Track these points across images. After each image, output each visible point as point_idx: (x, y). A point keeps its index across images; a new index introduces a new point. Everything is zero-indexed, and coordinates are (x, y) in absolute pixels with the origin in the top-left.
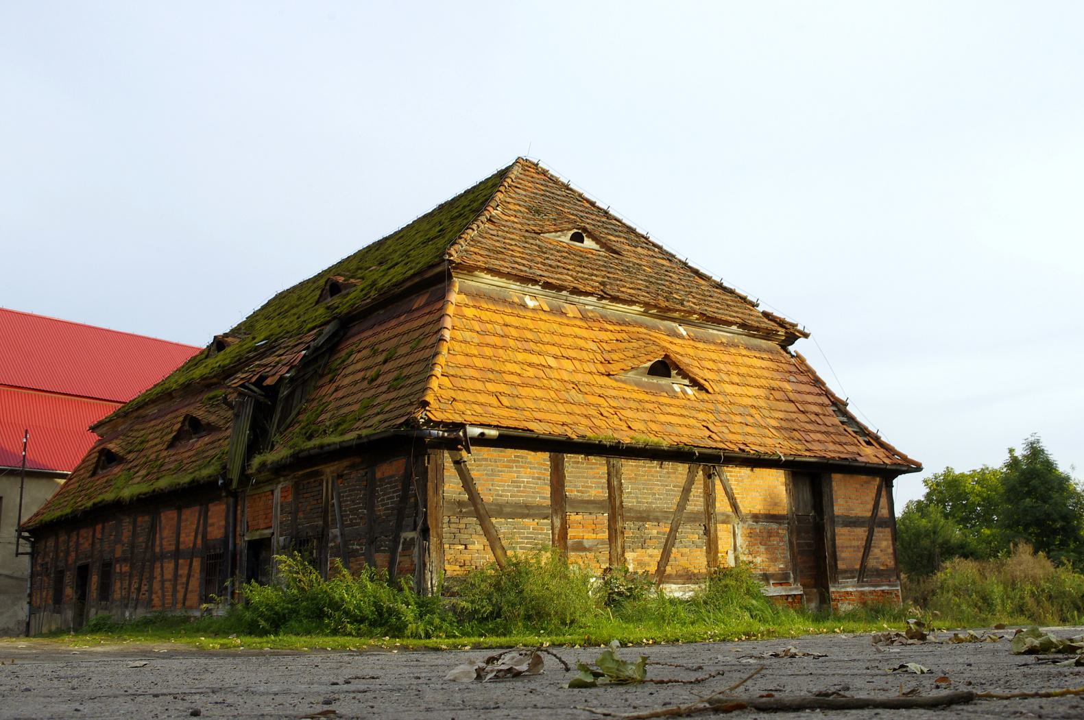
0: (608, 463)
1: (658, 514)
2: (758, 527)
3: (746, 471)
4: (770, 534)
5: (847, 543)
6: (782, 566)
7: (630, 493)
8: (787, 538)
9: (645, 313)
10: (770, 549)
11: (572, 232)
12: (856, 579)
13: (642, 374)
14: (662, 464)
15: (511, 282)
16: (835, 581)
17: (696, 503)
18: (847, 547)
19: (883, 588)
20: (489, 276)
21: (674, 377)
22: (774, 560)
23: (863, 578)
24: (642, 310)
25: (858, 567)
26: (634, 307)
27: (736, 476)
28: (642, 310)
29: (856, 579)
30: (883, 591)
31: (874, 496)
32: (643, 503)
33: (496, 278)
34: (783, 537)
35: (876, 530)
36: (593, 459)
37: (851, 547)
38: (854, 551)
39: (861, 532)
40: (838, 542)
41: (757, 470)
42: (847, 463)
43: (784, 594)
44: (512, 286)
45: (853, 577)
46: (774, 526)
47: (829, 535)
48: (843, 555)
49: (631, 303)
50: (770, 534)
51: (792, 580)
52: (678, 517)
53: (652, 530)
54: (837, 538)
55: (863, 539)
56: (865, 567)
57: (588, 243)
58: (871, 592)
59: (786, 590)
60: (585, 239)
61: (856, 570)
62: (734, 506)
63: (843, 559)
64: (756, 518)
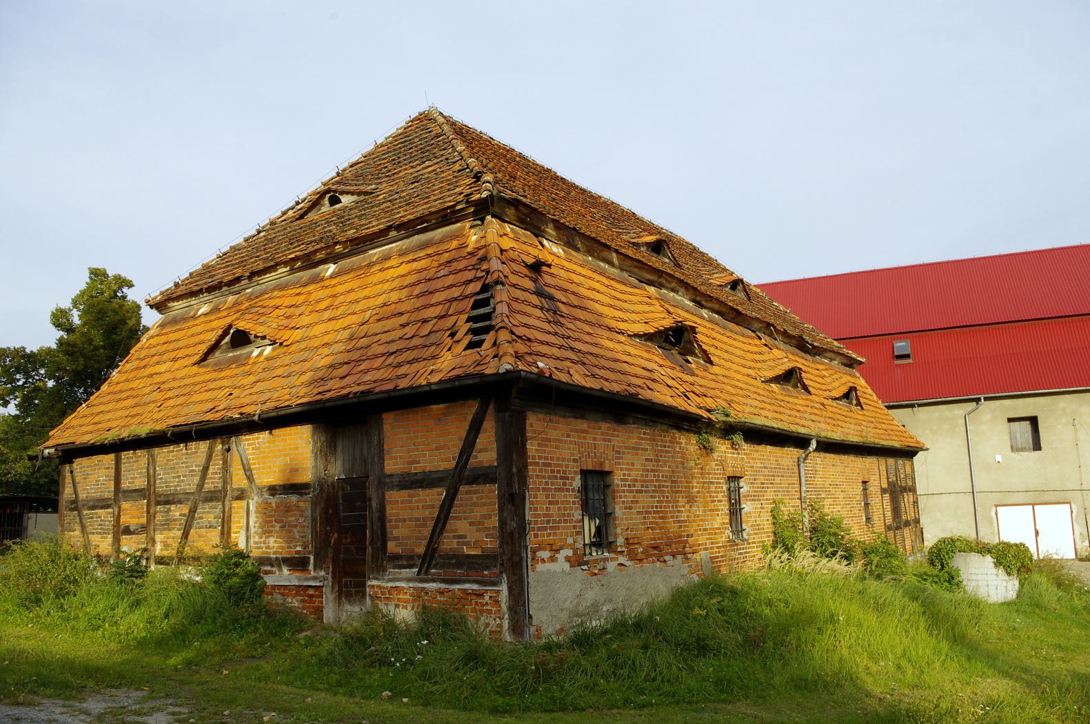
0: (148, 453)
1: (180, 496)
2: (273, 501)
3: (263, 436)
4: (288, 509)
5: (404, 514)
6: (299, 549)
7: (161, 479)
8: (309, 513)
9: (293, 271)
10: (286, 528)
11: (327, 199)
12: (416, 570)
13: (227, 351)
14: (186, 446)
15: (189, 300)
16: (380, 570)
17: (487, 453)
18: (404, 520)
19: (467, 586)
20: (176, 304)
21: (254, 341)
22: (290, 540)
23: (428, 568)
24: (288, 269)
25: (421, 550)
26: (281, 271)
27: (252, 445)
28: (288, 269)
29: (416, 570)
30: (464, 591)
31: (464, 434)
32: (171, 486)
33: (180, 302)
34: (303, 511)
35: (462, 488)
36: (139, 452)
37: (411, 520)
38: (417, 526)
39: (434, 496)
40: (390, 511)
41: (276, 432)
42: (321, 406)
43: (297, 584)
44: (193, 302)
45: (411, 567)
46: (294, 498)
47: (374, 504)
48: (395, 532)
49: (273, 268)
50: (288, 509)
51: (311, 567)
52: (462, 475)
53: (178, 512)
54: (388, 507)
55: (433, 507)
56: (434, 550)
57: (346, 200)
58: (441, 592)
59: (299, 579)
60: (341, 197)
61: (419, 556)
62: (250, 478)
63: (397, 539)
64: (273, 490)
